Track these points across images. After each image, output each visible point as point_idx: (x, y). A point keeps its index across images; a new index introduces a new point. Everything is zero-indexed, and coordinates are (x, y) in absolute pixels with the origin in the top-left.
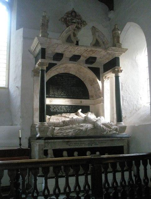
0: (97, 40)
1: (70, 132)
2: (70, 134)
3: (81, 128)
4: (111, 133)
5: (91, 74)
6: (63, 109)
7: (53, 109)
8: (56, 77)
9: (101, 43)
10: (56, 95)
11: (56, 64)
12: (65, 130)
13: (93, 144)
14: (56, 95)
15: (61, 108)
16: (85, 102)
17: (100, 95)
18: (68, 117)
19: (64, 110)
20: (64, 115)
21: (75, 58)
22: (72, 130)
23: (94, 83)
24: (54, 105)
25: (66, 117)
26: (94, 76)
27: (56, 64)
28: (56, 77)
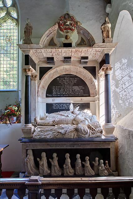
0: (82, 38)
1: (49, 135)
2: (48, 137)
3: (60, 131)
4: (94, 135)
5: (89, 75)
6: (64, 106)
7: (56, 107)
8: (58, 79)
9: (86, 42)
10: (58, 94)
11: (52, 68)
12: (44, 132)
13: (75, 146)
14: (58, 94)
15: (62, 106)
16: (85, 100)
17: (97, 93)
18: (64, 115)
19: (65, 108)
20: (61, 113)
21: (67, 59)
22: (51, 133)
23: (92, 82)
24: (56, 103)
25: (62, 115)
26: (92, 77)
27: (52, 68)
28: (58, 79)
